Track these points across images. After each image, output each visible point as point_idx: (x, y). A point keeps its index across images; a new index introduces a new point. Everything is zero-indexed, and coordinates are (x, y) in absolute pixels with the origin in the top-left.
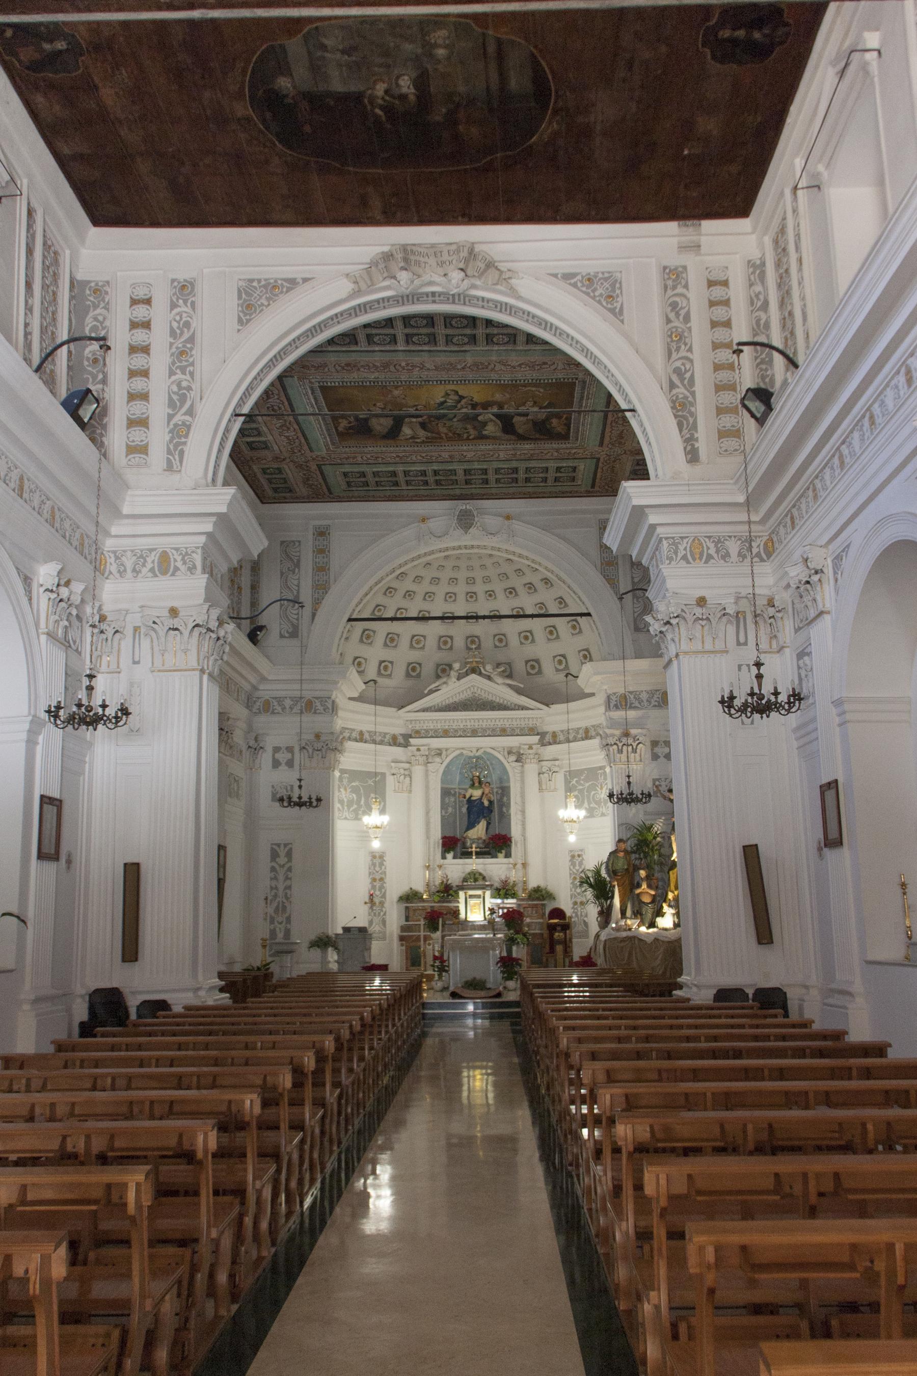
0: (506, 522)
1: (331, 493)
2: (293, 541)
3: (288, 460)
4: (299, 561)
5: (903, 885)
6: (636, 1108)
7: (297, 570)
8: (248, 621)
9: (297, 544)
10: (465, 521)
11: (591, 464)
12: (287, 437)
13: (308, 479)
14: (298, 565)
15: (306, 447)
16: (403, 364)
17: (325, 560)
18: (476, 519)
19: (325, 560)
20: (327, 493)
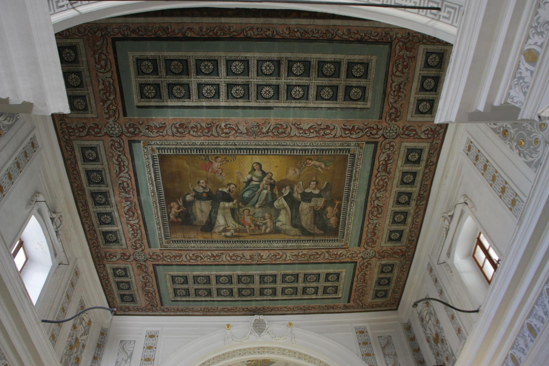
0: (289, 329)
1: (162, 305)
2: (130, 341)
3: (132, 258)
4: (132, 354)
5: (477, 311)
6: (288, 235)
7: (129, 360)
8: (87, 307)
9: (132, 342)
10: (259, 328)
11: (351, 266)
12: (132, 226)
13: (146, 286)
14: (130, 357)
15: (145, 241)
16: (223, 125)
17: (152, 354)
18: (267, 326)
19: (152, 354)
20: (159, 305)
